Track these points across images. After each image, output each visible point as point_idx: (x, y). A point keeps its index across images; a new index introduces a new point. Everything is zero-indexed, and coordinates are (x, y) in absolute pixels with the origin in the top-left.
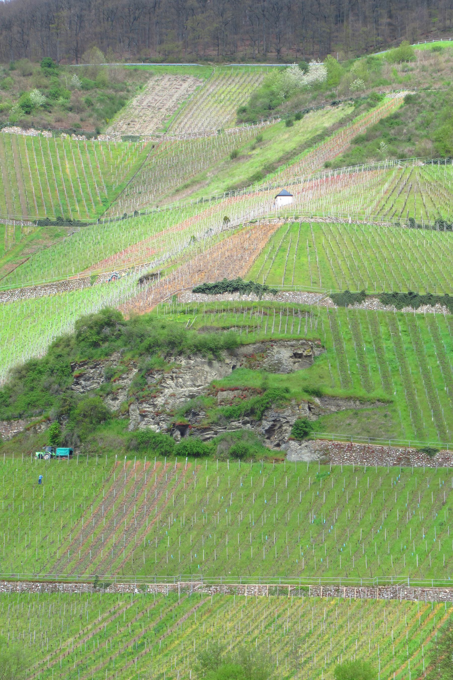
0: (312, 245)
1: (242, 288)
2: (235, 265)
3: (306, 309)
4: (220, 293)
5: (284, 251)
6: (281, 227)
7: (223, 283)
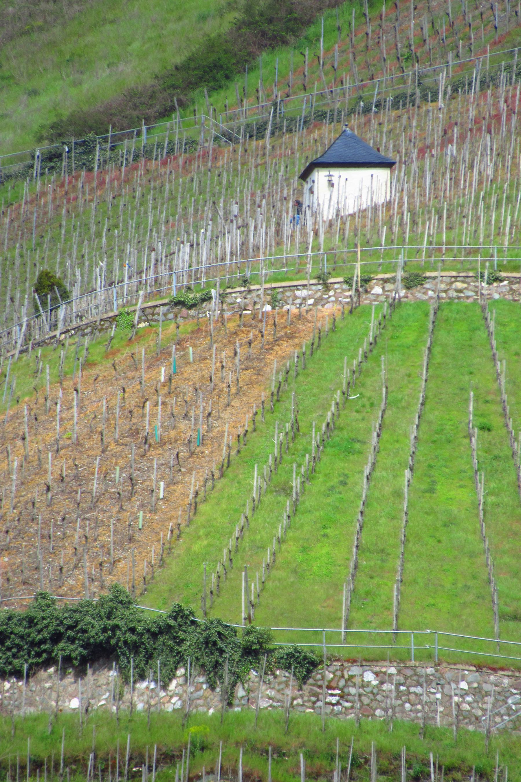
0: (496, 421)
1: (135, 648)
2: (97, 524)
3: (469, 756)
4: (18, 674)
5: (350, 451)
6: (334, 329)
7: (31, 621)
